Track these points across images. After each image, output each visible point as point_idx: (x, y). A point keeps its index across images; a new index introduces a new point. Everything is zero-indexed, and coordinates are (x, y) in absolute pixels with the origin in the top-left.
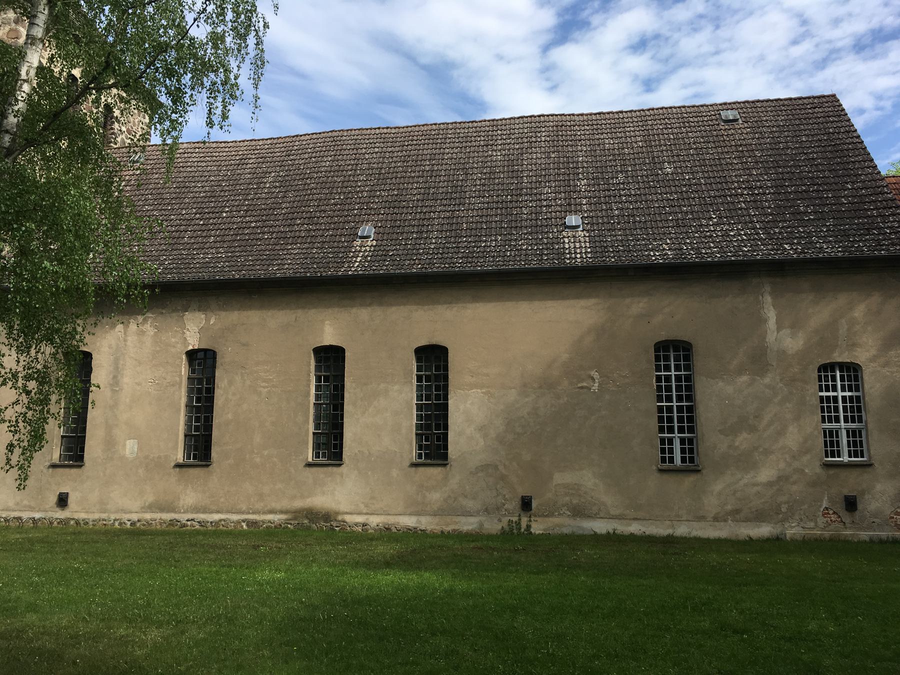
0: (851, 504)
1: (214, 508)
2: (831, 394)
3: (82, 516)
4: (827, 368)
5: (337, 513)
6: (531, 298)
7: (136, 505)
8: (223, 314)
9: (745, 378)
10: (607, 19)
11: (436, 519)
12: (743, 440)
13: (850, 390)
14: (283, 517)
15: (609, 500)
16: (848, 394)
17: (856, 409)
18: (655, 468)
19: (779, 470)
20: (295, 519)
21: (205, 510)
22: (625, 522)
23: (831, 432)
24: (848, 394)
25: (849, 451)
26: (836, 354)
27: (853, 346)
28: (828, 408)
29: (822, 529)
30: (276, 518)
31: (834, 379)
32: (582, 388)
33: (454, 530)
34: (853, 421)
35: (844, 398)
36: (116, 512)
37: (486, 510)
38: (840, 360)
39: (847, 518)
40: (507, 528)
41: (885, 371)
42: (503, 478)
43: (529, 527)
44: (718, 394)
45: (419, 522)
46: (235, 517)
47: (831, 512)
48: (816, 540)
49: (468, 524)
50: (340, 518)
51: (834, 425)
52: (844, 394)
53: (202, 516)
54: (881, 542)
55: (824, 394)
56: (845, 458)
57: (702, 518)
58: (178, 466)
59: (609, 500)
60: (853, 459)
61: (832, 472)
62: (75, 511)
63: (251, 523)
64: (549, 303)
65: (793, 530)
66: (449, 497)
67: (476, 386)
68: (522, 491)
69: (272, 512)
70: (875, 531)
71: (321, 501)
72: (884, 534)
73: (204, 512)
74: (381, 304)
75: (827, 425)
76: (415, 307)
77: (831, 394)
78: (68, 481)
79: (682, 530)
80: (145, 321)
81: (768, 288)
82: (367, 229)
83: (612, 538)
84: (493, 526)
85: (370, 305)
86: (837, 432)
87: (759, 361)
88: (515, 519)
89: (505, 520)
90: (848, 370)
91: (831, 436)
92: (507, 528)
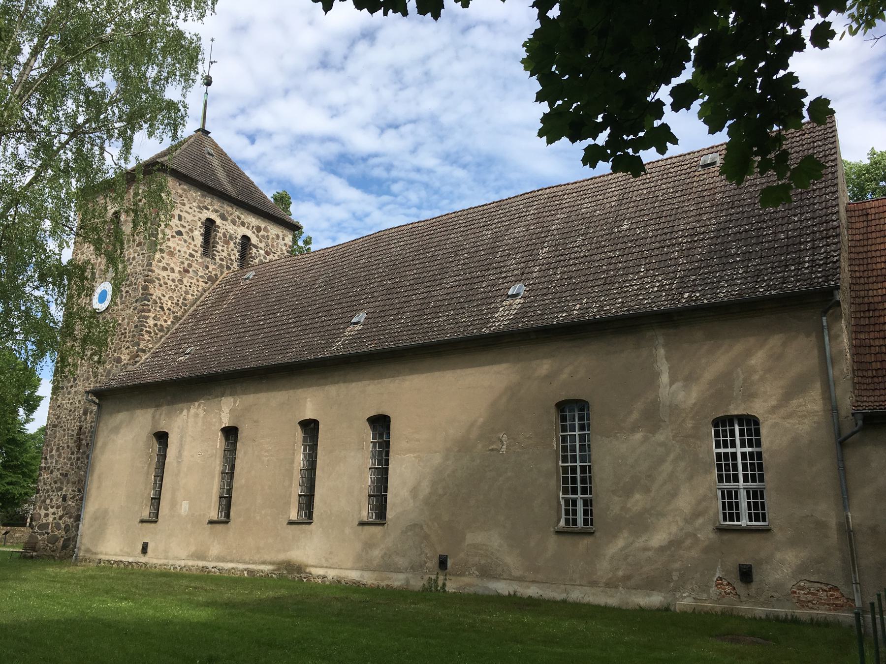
0: (746, 574)
1: (229, 558)
2: (730, 450)
3: (155, 561)
4: (723, 423)
5: (307, 566)
6: (454, 367)
7: (183, 554)
8: (244, 397)
9: (638, 436)
10: (244, 162)
11: (375, 575)
12: (638, 501)
13: (750, 446)
14: (270, 567)
15: (511, 561)
16: (747, 450)
17: (756, 467)
18: (552, 529)
19: (670, 534)
20: (278, 569)
21: (223, 560)
22: (525, 584)
23: (730, 493)
24: (747, 450)
25: (750, 514)
26: (732, 407)
27: (750, 396)
28: (725, 466)
29: (716, 602)
30: (267, 568)
31: (732, 434)
32: (492, 450)
33: (388, 586)
34: (754, 480)
35: (744, 455)
36: (173, 559)
37: (412, 568)
38: (736, 413)
39: (740, 588)
40: (427, 586)
41: (787, 424)
42: (426, 537)
43: (444, 585)
44: (615, 453)
45: (362, 576)
46: (241, 566)
47: (725, 583)
48: (707, 613)
49: (397, 580)
50: (308, 570)
51: (732, 485)
52: (744, 450)
53: (221, 565)
54: (777, 619)
55: (722, 450)
56: (744, 522)
57: (593, 584)
58: (211, 522)
59: (511, 561)
60: (728, 523)
61: (726, 537)
62: (153, 559)
63: (250, 572)
64: (469, 371)
65: (685, 601)
66: (385, 554)
67: (409, 451)
68: (441, 551)
69: (264, 563)
70: (773, 607)
71: (297, 555)
72: (781, 611)
73: (223, 561)
74: (345, 382)
75: (725, 485)
76: (367, 382)
77: (730, 450)
78: (148, 534)
79: (576, 595)
80: (199, 405)
81: (661, 340)
82: (517, 288)
83: (515, 602)
84: (417, 583)
85: (337, 383)
86: (736, 493)
87: (652, 418)
88: (433, 577)
89: (427, 577)
90: (748, 424)
91: (730, 497)
92: (427, 586)
